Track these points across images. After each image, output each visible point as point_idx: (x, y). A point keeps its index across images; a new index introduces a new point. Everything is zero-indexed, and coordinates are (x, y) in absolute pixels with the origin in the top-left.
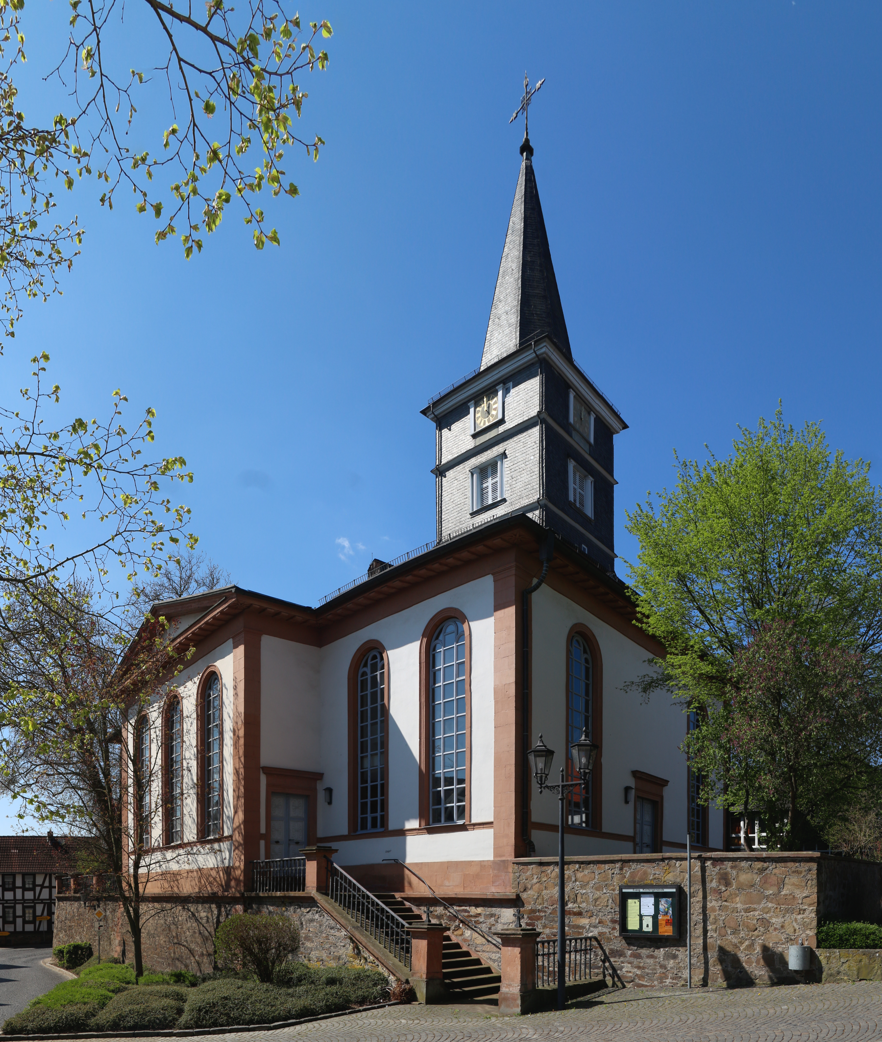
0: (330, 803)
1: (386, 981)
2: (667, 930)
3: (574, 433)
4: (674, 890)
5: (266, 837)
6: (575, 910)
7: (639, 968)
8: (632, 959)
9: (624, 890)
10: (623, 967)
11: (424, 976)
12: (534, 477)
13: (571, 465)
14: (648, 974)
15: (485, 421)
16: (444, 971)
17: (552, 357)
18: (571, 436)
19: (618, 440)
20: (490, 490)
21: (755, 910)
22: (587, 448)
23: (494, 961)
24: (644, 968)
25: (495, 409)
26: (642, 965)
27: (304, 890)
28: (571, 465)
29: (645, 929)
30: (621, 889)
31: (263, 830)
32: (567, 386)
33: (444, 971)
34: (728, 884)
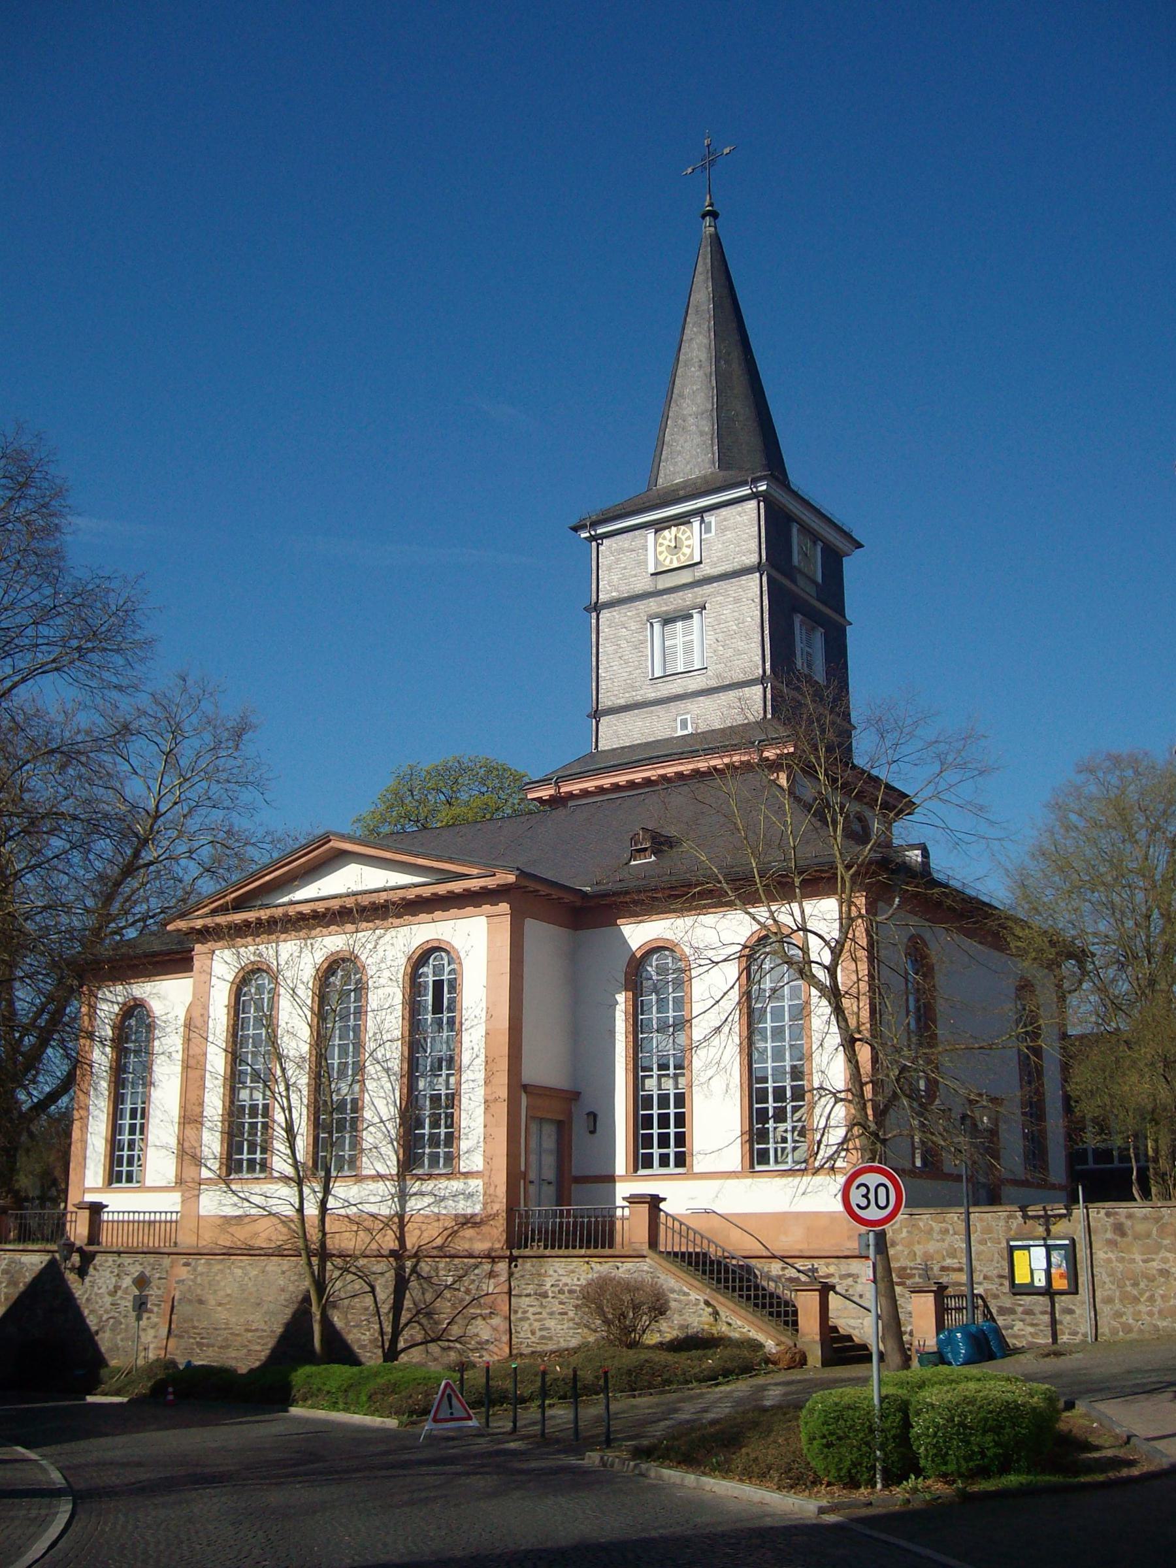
0: (593, 1132)
1: (761, 1346)
2: (1060, 1284)
3: (799, 577)
4: (1067, 1242)
5: (525, 1175)
6: (955, 1266)
7: (1032, 1325)
8: (1024, 1316)
9: (1012, 1243)
10: (1014, 1325)
11: (818, 1338)
12: (752, 645)
13: (798, 619)
14: (1042, 1331)
15: (672, 559)
16: (835, 1346)
17: (776, 495)
18: (794, 581)
19: (851, 566)
20: (680, 650)
21: (1153, 1260)
22: (812, 590)
23: (854, 1328)
24: (1036, 1325)
25: (688, 546)
26: (1035, 1322)
27: (611, 1247)
28: (798, 619)
29: (1037, 1283)
30: (1008, 1243)
31: (523, 1168)
32: (790, 518)
33: (835, 1346)
34: (1123, 1234)
